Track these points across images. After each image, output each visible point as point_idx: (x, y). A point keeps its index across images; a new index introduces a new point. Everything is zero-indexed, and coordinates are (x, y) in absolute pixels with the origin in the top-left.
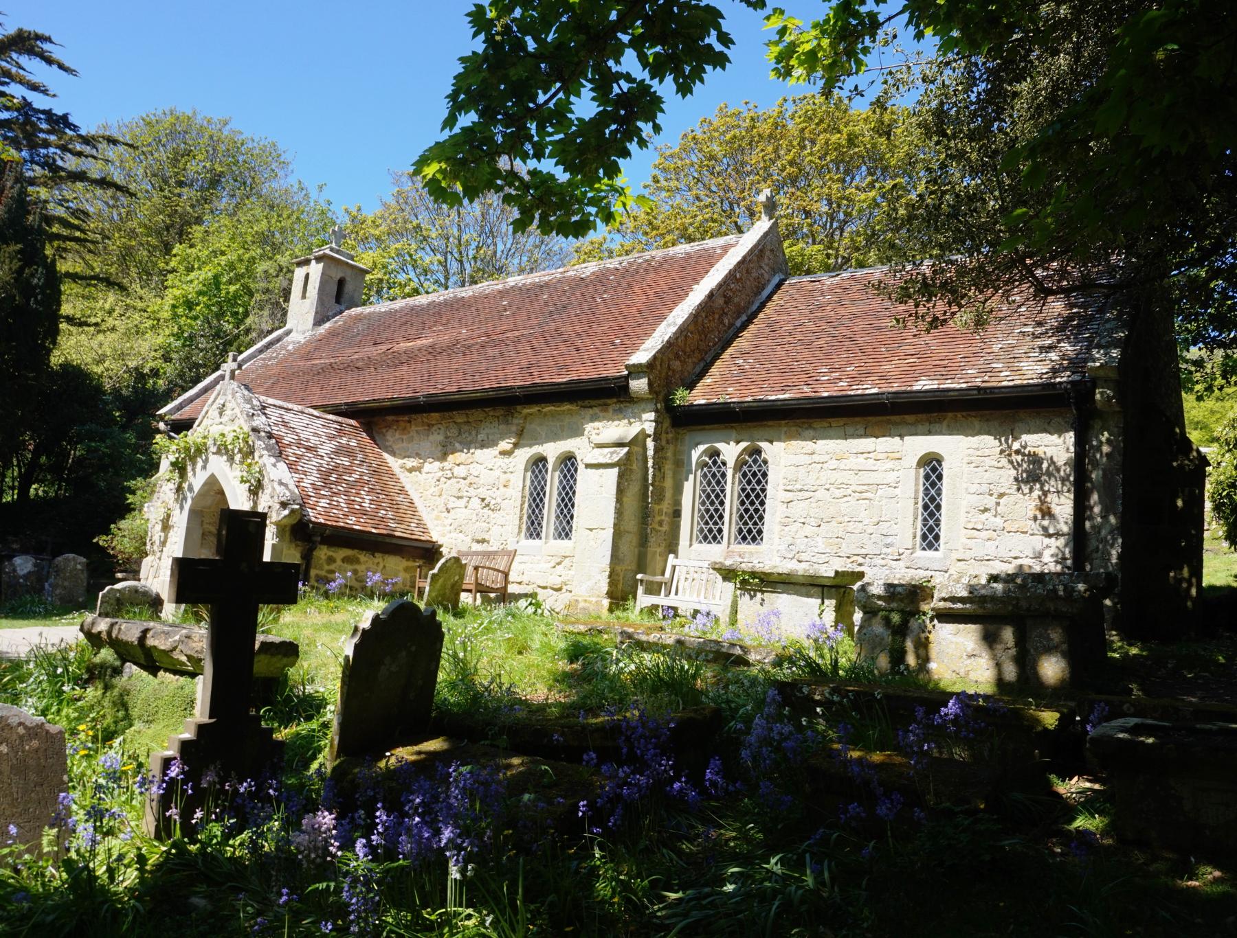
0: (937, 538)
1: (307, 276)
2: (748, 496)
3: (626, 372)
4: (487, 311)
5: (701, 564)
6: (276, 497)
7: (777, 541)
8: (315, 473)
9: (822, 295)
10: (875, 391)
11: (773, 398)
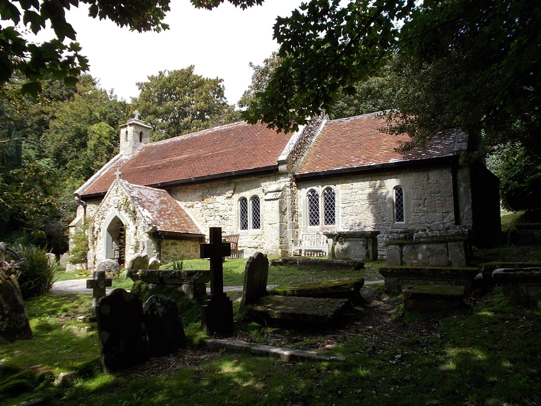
0: (402, 217)
1: (127, 132)
2: (328, 207)
3: (277, 164)
4: (209, 142)
5: (314, 233)
6: (146, 223)
7: (341, 223)
8: (156, 212)
9: (345, 127)
10: (374, 164)
11: (335, 169)
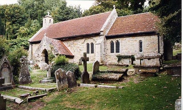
0: (142, 50)
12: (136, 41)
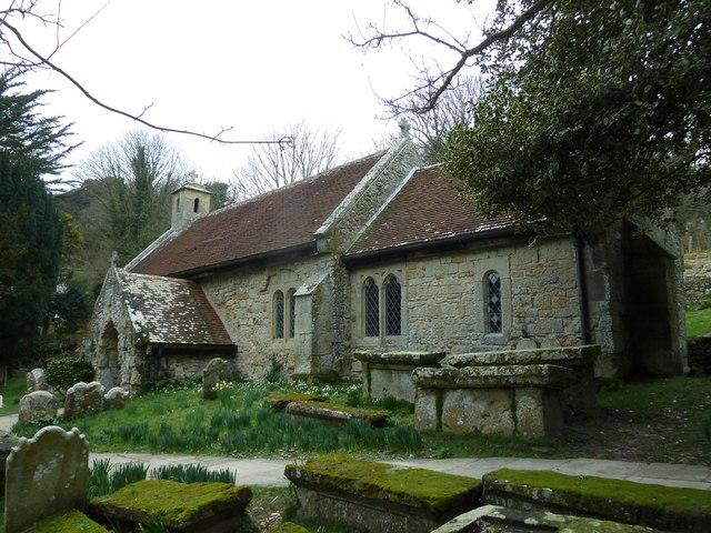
12: (470, 274)
